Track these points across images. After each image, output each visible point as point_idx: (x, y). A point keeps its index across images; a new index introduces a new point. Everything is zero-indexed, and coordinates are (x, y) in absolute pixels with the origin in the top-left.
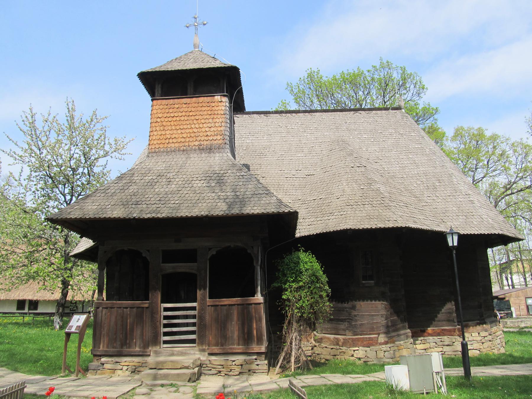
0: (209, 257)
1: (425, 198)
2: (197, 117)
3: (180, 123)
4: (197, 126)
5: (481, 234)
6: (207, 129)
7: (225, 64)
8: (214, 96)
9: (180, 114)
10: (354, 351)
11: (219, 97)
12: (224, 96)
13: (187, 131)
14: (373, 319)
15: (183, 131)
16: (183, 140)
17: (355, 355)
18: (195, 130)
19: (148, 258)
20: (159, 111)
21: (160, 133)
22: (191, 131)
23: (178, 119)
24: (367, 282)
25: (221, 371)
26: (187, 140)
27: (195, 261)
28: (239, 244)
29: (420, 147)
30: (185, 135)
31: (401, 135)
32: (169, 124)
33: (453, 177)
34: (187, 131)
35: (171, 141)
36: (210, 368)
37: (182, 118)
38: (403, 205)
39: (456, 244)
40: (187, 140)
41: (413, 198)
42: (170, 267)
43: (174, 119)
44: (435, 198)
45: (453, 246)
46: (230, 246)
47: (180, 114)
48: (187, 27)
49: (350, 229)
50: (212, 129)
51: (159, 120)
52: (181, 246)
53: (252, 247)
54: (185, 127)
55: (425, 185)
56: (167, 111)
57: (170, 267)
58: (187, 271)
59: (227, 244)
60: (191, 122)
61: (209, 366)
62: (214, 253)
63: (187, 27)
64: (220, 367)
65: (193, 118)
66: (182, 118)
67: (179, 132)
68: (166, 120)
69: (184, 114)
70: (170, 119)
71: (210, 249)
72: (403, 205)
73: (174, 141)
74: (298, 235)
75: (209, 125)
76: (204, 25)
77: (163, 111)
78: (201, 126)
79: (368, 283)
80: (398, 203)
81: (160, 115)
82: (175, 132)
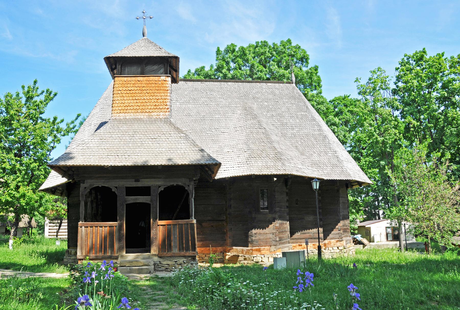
0: (159, 192)
1: (306, 153)
2: (148, 92)
3: (135, 95)
4: (148, 98)
5: (341, 180)
6: (156, 101)
7: (169, 54)
8: (160, 76)
9: (136, 89)
10: (254, 257)
11: (164, 77)
12: (168, 76)
13: (141, 101)
14: (267, 236)
15: (138, 101)
16: (138, 108)
17: (254, 260)
18: (147, 101)
19: (116, 192)
20: (120, 85)
21: (121, 102)
22: (144, 101)
23: (134, 92)
24: (264, 211)
25: (167, 268)
26: (141, 108)
27: (149, 195)
28: (180, 184)
29: (304, 114)
30: (139, 104)
31: (291, 104)
32: (127, 95)
33: (326, 138)
34: (141, 101)
35: (129, 108)
36: (160, 267)
37: (137, 92)
38: (290, 158)
39: (318, 188)
40: (141, 108)
41: (298, 153)
42: (132, 199)
43: (131, 92)
44: (312, 153)
45: (316, 189)
46: (173, 185)
47: (136, 89)
48: (137, 19)
49: (254, 174)
50: (159, 101)
51: (119, 92)
52: (139, 184)
53: (189, 186)
54: (139, 98)
55: (307, 143)
56: (126, 85)
57: (132, 199)
58: (144, 201)
59: (172, 184)
60: (144, 94)
61: (159, 265)
62: (163, 189)
63: (137, 19)
64: (167, 266)
65: (145, 92)
66: (137, 92)
67: (135, 101)
68: (125, 92)
69: (138, 88)
70: (128, 92)
71: (159, 187)
72: (290, 158)
73: (132, 108)
74: (217, 178)
75: (157, 98)
76: (151, 18)
77: (123, 86)
78: (151, 98)
79: (264, 212)
80: (287, 157)
81: (121, 89)
82: (132, 101)
